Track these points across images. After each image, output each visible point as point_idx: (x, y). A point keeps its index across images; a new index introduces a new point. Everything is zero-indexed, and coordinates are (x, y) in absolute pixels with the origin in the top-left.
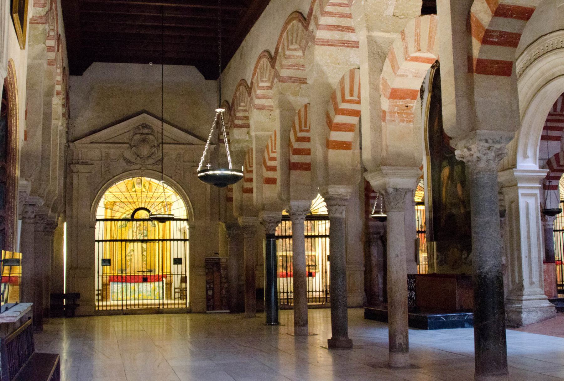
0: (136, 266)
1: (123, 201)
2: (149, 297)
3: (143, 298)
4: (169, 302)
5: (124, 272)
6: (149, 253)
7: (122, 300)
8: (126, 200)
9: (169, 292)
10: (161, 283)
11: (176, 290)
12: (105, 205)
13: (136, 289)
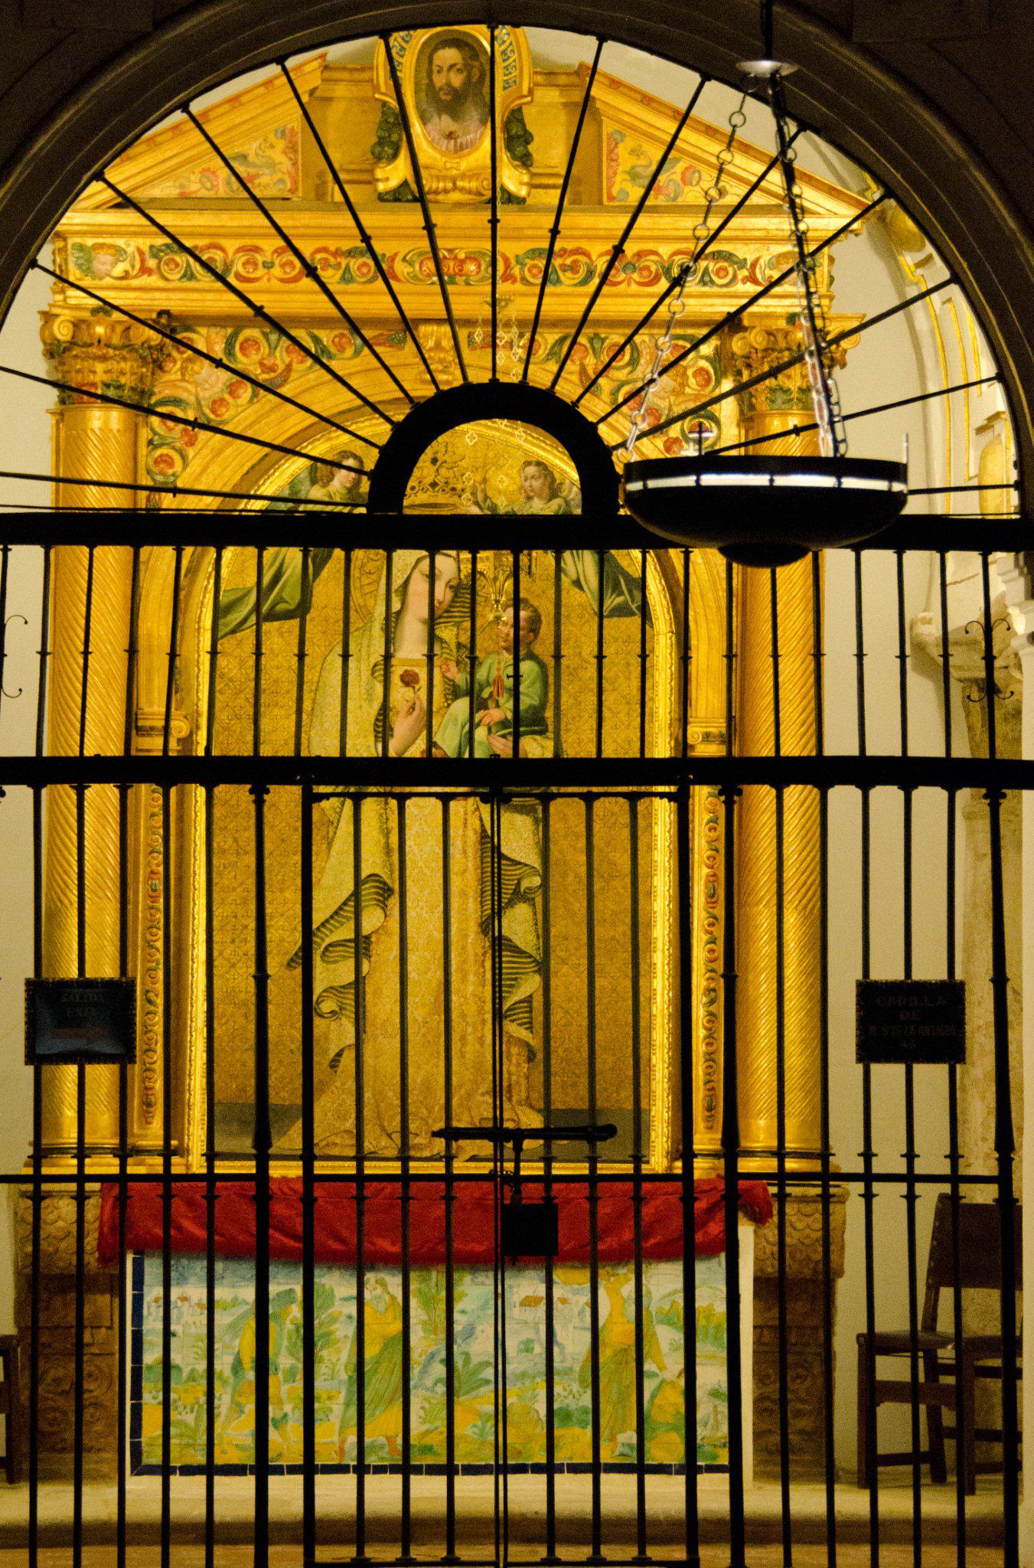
0: (426, 1068)
1: (273, 306)
2: (575, 1444)
3: (501, 1447)
4: (808, 1501)
5: (290, 1139)
6: (568, 926)
7: (690, 1470)
8: (304, 299)
9: (802, 1388)
10: (710, 1275)
11: (892, 1368)
12: (54, 351)
13: (425, 1342)
